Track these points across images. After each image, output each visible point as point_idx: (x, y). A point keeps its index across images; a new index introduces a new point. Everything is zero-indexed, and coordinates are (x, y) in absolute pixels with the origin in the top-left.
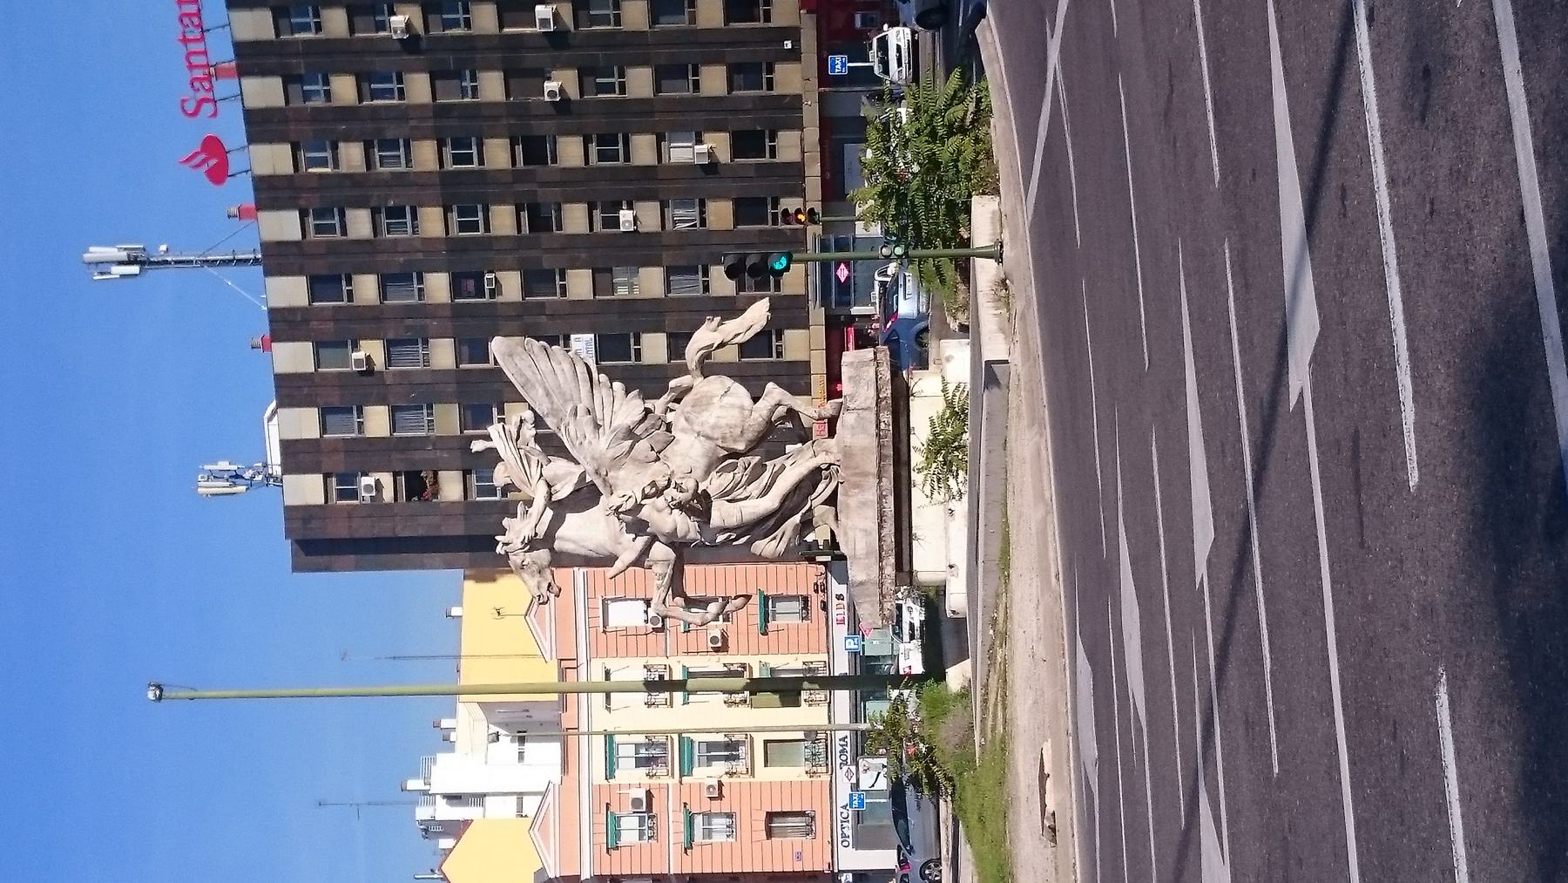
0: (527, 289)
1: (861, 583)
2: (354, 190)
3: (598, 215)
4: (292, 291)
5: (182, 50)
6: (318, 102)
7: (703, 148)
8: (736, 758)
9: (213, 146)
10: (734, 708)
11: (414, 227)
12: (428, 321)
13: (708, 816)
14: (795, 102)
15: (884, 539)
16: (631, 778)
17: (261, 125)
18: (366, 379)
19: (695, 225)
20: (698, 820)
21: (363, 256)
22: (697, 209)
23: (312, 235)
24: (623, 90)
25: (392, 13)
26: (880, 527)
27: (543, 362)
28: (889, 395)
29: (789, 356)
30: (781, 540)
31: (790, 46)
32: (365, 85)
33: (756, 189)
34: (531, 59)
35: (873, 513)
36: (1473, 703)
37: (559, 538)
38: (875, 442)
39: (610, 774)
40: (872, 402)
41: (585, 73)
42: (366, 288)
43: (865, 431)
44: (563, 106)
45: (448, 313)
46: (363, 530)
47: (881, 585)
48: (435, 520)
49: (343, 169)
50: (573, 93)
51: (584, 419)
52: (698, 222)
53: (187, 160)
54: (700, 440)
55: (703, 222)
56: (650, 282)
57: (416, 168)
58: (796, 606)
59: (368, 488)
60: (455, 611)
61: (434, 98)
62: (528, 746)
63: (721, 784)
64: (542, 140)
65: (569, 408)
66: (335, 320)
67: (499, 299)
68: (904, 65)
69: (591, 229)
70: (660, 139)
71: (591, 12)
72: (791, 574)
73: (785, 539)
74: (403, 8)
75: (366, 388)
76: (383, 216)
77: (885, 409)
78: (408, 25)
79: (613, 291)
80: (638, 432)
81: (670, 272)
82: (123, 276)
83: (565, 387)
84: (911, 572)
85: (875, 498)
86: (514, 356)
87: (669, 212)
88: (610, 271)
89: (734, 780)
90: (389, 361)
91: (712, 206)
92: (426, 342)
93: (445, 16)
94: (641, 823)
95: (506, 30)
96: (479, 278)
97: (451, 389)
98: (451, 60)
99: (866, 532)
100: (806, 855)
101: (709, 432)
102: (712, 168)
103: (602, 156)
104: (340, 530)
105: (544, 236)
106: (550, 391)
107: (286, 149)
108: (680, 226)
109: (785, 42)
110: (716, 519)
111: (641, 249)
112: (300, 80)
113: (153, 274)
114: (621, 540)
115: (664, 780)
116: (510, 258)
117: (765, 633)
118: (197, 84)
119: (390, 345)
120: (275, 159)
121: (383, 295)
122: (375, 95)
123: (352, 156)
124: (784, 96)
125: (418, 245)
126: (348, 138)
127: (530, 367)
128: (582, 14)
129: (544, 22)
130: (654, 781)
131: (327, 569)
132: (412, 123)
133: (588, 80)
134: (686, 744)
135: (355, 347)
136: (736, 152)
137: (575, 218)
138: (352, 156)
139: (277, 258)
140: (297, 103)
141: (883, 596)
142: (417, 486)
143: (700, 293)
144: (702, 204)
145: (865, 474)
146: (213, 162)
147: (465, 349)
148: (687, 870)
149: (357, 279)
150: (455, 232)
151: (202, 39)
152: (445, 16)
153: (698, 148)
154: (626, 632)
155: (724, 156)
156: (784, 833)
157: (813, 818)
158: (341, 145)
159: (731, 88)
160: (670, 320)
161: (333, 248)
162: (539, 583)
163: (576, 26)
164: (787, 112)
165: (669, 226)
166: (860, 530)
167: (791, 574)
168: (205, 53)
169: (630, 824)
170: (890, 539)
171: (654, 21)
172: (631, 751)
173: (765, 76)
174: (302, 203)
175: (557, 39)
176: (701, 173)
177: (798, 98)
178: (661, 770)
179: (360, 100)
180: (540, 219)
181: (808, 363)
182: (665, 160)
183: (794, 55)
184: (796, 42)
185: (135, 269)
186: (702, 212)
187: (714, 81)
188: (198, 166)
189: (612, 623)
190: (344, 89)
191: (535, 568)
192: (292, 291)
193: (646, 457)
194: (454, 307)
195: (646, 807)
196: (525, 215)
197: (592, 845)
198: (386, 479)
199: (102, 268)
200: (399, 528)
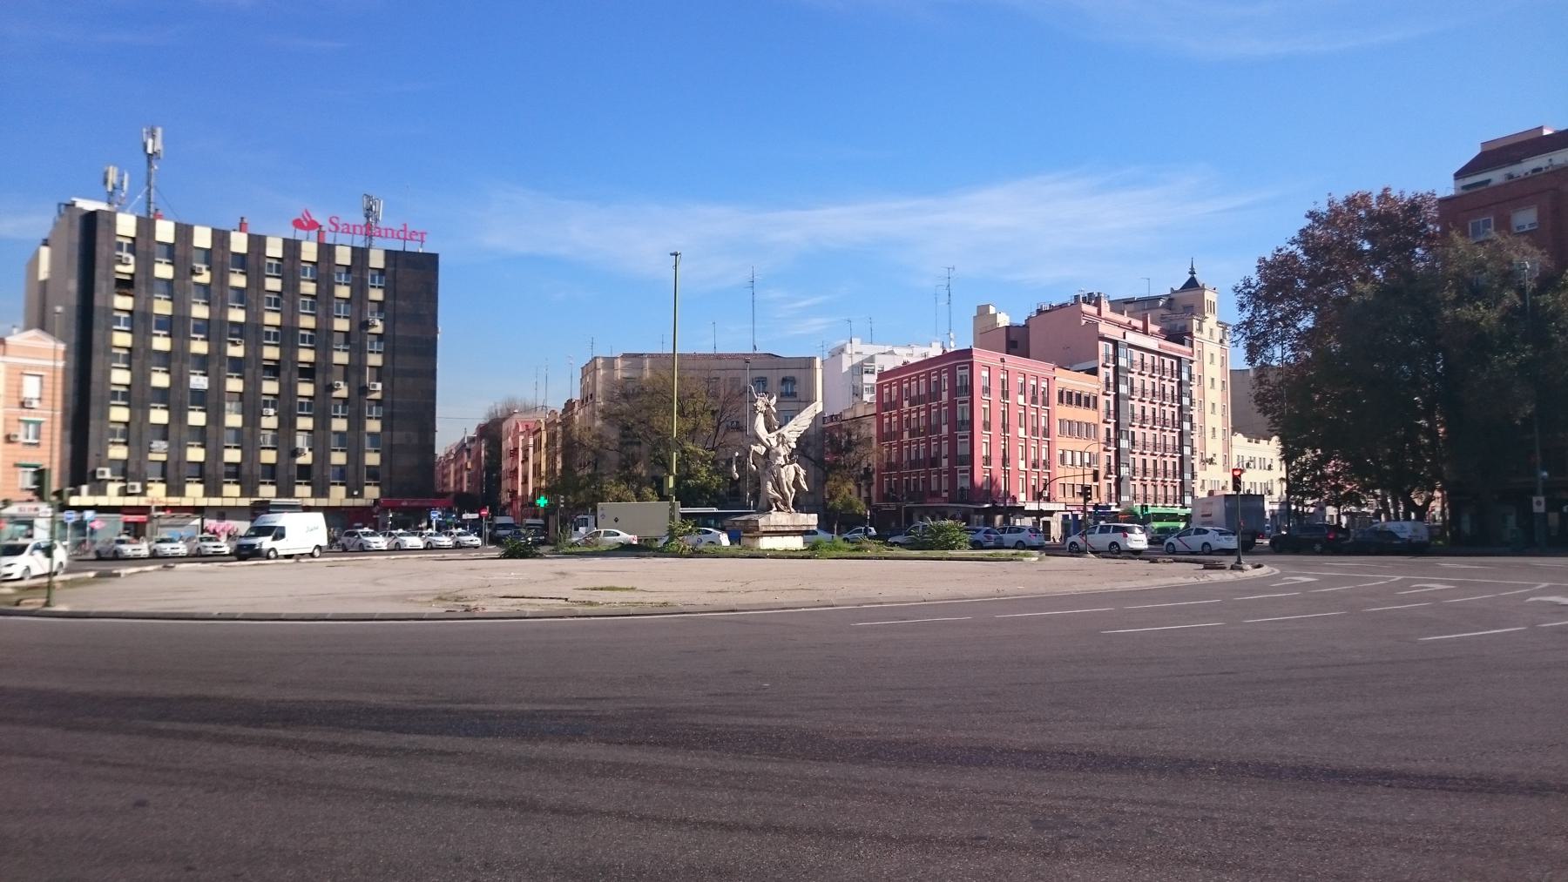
0: (233, 359)
2: (291, 285)
3: (271, 398)
11: (303, 314)
12: (219, 306)
18: (188, 271)
21: (256, 280)
23: (268, 261)
25: (381, 320)
33: (281, 474)
34: (354, 377)
35: (784, 523)
36: (813, 765)
41: (345, 401)
42: (238, 281)
48: (104, 291)
50: (335, 394)
55: (263, 448)
66: (222, 263)
70: (309, 431)
75: (185, 269)
78: (374, 326)
84: (762, 536)
87: (270, 433)
95: (368, 369)
97: (181, 313)
102: (295, 453)
105: (297, 374)
107: (314, 259)
113: (145, 158)
116: (251, 354)
118: (346, 226)
119: (206, 287)
121: (234, 288)
123: (309, 288)
125: (260, 310)
126: (318, 288)
129: (374, 386)
132: (325, 320)
133: (341, 402)
136: (301, 466)
137: (270, 387)
138: (309, 288)
142: (125, 286)
144: (273, 449)
146: (305, 223)
147: (199, 323)
154: (20, 387)
155: (300, 460)
164: (176, 489)
165: (263, 432)
174: (286, 260)
175: (364, 390)
182: (298, 433)
183: (349, 495)
184: (357, 497)
186: (268, 448)
194: (152, 313)
198: (130, 269)
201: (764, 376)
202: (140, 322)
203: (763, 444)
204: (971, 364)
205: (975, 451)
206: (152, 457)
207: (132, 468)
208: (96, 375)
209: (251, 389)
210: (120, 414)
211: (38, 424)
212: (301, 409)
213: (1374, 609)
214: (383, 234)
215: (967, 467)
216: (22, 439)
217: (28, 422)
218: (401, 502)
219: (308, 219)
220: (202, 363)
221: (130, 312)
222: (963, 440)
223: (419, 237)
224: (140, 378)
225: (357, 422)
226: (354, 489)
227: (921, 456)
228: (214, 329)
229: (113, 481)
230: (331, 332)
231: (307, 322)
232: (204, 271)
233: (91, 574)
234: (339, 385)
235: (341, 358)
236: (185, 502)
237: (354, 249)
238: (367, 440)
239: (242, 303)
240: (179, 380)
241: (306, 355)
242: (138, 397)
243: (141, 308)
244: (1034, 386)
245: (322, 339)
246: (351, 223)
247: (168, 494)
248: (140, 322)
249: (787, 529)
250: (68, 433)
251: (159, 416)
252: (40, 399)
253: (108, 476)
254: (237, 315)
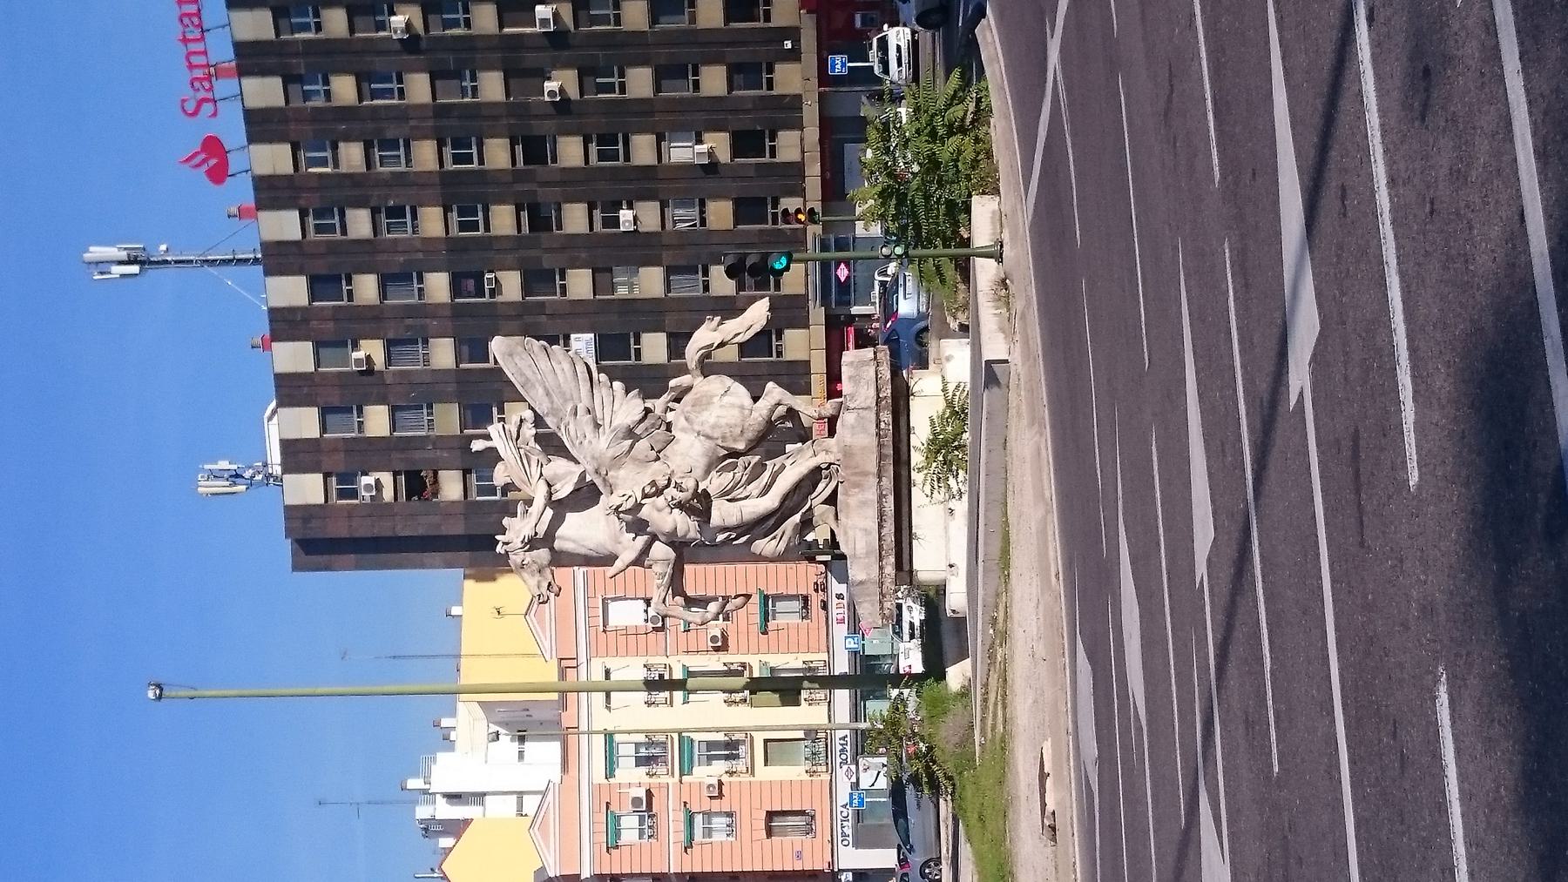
0: (527, 289)
1: (861, 583)
2: (354, 190)
3: (598, 215)
4: (292, 291)
5: (182, 50)
6: (318, 102)
7: (703, 148)
8: (736, 757)
9: (213, 146)
10: (734, 707)
11: (414, 227)
12: (428, 321)
13: (708, 815)
14: (795, 102)
15: (884, 538)
16: (631, 777)
17: (261, 125)
18: (366, 379)
19: (695, 225)
21: (363, 255)
22: (697, 208)
23: (312, 235)
24: (623, 90)
25: (392, 13)
26: (880, 527)
27: (543, 362)
28: (889, 395)
29: (789, 356)
30: (781, 539)
31: (790, 46)
32: (365, 85)
33: (756, 189)
34: (531, 59)
35: (873, 513)
37: (559, 537)
38: (875, 441)
39: (610, 773)
40: (872, 402)
41: (585, 73)
42: (366, 288)
43: (865, 430)
44: (563, 106)
45: (448, 313)
46: (363, 530)
47: (881, 584)
48: (435, 519)
49: (343, 169)
50: (573, 93)
51: (584, 418)
52: (698, 222)
53: (187, 160)
54: (700, 440)
55: (703, 222)
56: (650, 282)
57: (416, 168)
58: (796, 605)
59: (368, 487)
60: (455, 611)
61: (434, 98)
62: (528, 745)
63: (721, 784)
64: (542, 140)
65: (569, 407)
67: (499, 299)
68: (904, 65)
69: (591, 228)
70: (660, 138)
71: (591, 12)
72: (791, 573)
73: (785, 538)
74: (403, 8)
75: (366, 387)
76: (383, 215)
77: (885, 409)
78: (408, 25)
79: (613, 291)
80: (638, 431)
81: (670, 271)
82: (123, 276)
83: (565, 387)
84: (911, 571)
85: (875, 498)
86: (514, 356)
87: (669, 212)
88: (610, 270)
89: (734, 779)
90: (389, 360)
91: (712, 206)
92: (426, 342)
93: (445, 16)
94: (641, 822)
95: (506, 30)
96: (479, 278)
97: (451, 388)
98: (451, 60)
99: (866, 531)
100: (806, 854)
101: (709, 431)
102: (712, 168)
103: (602, 156)
104: (340, 530)
105: (544, 235)
106: (550, 391)
107: (286, 149)
108: (680, 226)
109: (785, 42)
110: (716, 519)
111: (641, 249)
112: (300, 80)
113: (153, 273)
114: (621, 539)
115: (664, 779)
116: (510, 258)
117: (765, 633)
118: (197, 84)
119: (390, 345)
121: (383, 294)
122: (375, 94)
123: (352, 156)
124: (784, 96)
125: (418, 245)
126: (348, 138)
127: (530, 366)
128: (582, 14)
129: (544, 22)
130: (654, 780)
131: (327, 568)
132: (412, 123)
133: (588, 80)
134: (686, 744)
135: (355, 347)
136: (736, 151)
137: (575, 218)
138: (352, 156)
139: (277, 258)
140: (297, 103)
141: (883, 595)
142: (417, 485)
143: (700, 293)
144: (702, 204)
145: (865, 474)
146: (213, 162)
147: (465, 349)
148: (687, 869)
149: (357, 278)
150: (455, 231)
151: (202, 39)
152: (445, 16)
153: (698, 148)
154: (626, 632)
155: (724, 156)
156: (784, 832)
158: (341, 145)
159: (731, 88)
160: (670, 320)
161: (333, 248)
162: (539, 582)
163: (576, 26)
164: (787, 111)
165: (669, 225)
166: (860, 529)
167: (791, 573)
168: (205, 53)
169: (630, 823)
170: (890, 539)
171: (654, 21)
172: (631, 750)
173: (765, 76)
174: (302, 202)
175: (557, 39)
176: (701, 173)
177: (798, 98)
178: (661, 770)
179: (360, 100)
180: (540, 219)
181: (808, 363)
182: (665, 160)
183: (794, 55)
184: (796, 42)
185: (135, 269)
186: (702, 212)
187: (714, 81)
188: (198, 166)
189: (612, 623)
190: (344, 89)
191: (535, 567)
192: (292, 291)
193: (646, 456)
194: (454, 307)
195: (646, 806)
196: (525, 215)
197: (592, 844)
198: (386, 478)
199: (102, 267)
200: (399, 527)
219: (202, 156)
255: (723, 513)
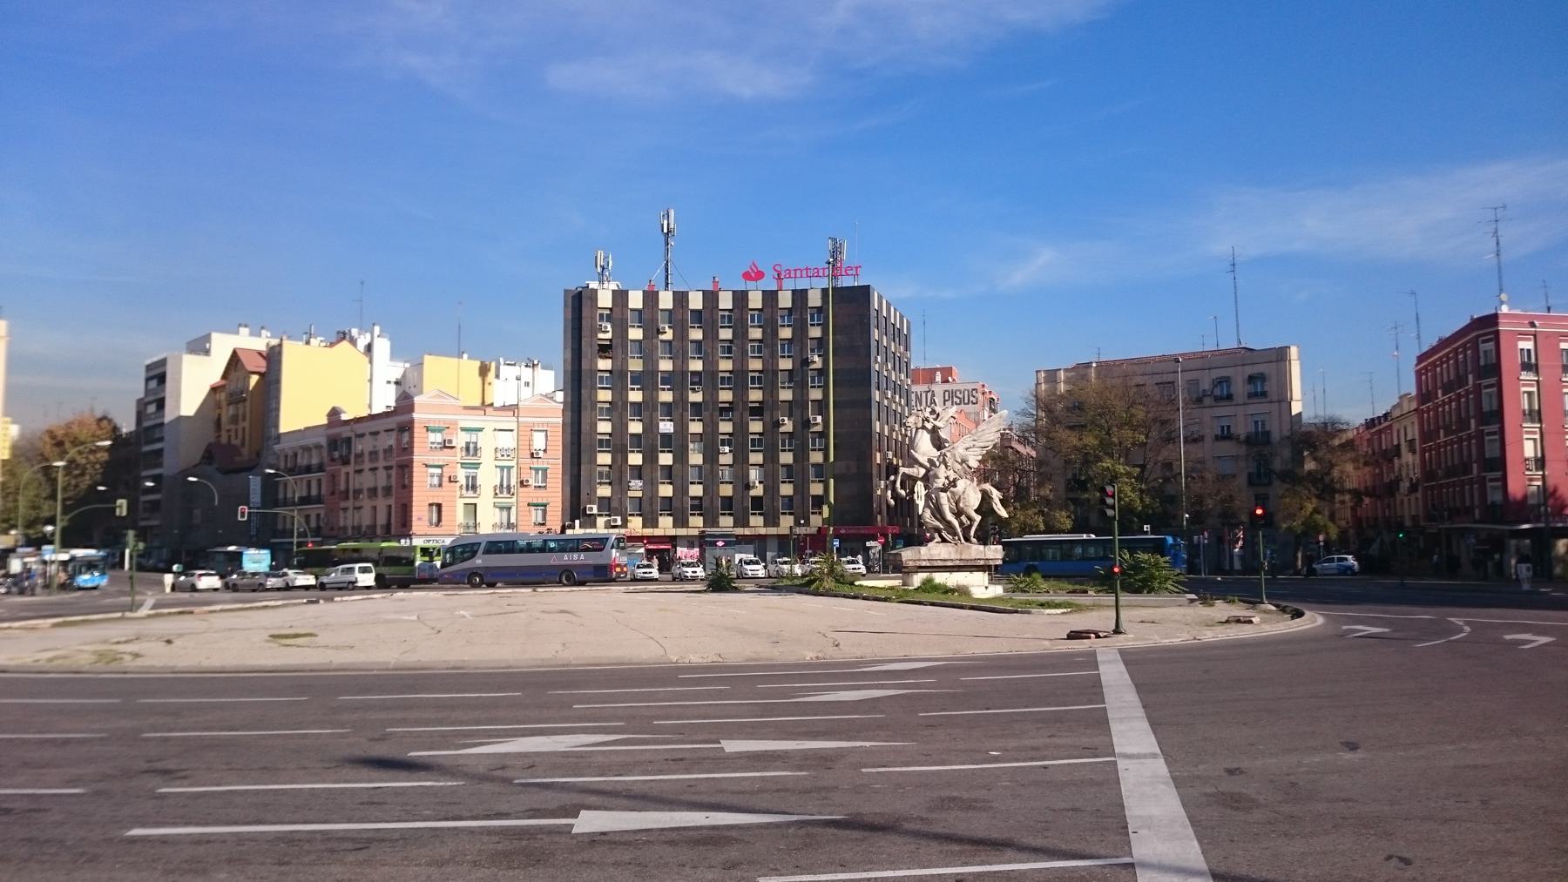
0: (694, 404)
4: (696, 302)
5: (803, 267)
6: (780, 323)
7: (757, 484)
8: (467, 489)
9: (760, 275)
10: (493, 489)
11: (723, 358)
13: (441, 477)
14: (776, 524)
16: (460, 440)
17: (770, 297)
20: (439, 471)
21: (711, 334)
23: (721, 313)
25: (819, 356)
27: (995, 429)
29: (661, 519)
32: (787, 342)
34: (797, 412)
35: (946, 557)
38: (973, 558)
39: (463, 429)
42: (696, 334)
43: (978, 554)
44: (777, 424)
46: (586, 323)
47: (919, 560)
49: (750, 330)
50: (782, 429)
53: (753, 264)
55: (722, 483)
56: (696, 458)
58: (540, 520)
59: (606, 327)
60: (465, 356)
61: (781, 371)
62: (393, 386)
63: (456, 482)
67: (690, 392)
70: (760, 466)
72: (556, 518)
74: (821, 360)
75: (652, 331)
78: (814, 362)
80: (964, 465)
81: (700, 467)
82: (663, 225)
84: (917, 572)
87: (727, 468)
89: (458, 489)
90: (662, 341)
91: (730, 486)
92: (671, 358)
94: (439, 443)
99: (939, 555)
100: (420, 523)
102: (748, 487)
104: (586, 312)
108: (720, 472)
111: (711, 456)
112: (790, 315)
113: (663, 238)
115: (459, 455)
116: (708, 398)
117: (529, 505)
118: (816, 271)
119: (670, 342)
120: (756, 301)
122: (783, 346)
123: (756, 333)
126: (764, 333)
129: (815, 419)
130: (459, 450)
131: (565, 305)
133: (787, 436)
134: (477, 466)
135: (670, 327)
137: (726, 427)
139: (711, 297)
140: (779, 312)
141: (915, 561)
142: (605, 350)
144: (731, 483)
145: (961, 554)
146: (753, 275)
147: (667, 375)
148: (415, 464)
149: (701, 331)
151: (807, 276)
153: (757, 482)
155: (753, 493)
156: (431, 512)
157: (437, 525)
158: (761, 330)
159: (783, 497)
160: (678, 466)
161: (714, 322)
164: (772, 521)
165: (721, 468)
167: (556, 518)
168: (801, 277)
169: (438, 438)
170: (936, 564)
171: (813, 465)
172: (474, 440)
173: (788, 511)
174: (765, 310)
175: (807, 424)
176: (745, 482)
177: (778, 525)
178: (464, 453)
179: (781, 339)
180: (726, 411)
181: (657, 527)
182: (750, 467)
185: (665, 231)
186: (727, 483)
187: (786, 490)
188: (752, 269)
189: (535, 434)
190: (786, 333)
192: (696, 302)
195: (446, 445)
196: (727, 405)
197: (429, 421)
198: (609, 336)
199: (666, 216)
200: (586, 339)
201: (1261, 370)
202: (618, 379)
203: (922, 465)
204: (1497, 333)
205: (1508, 448)
206: (631, 494)
207: (614, 504)
208: (585, 427)
209: (709, 430)
210: (604, 459)
211: (545, 471)
212: (601, 446)
213: (867, 744)
214: (821, 274)
215: (1498, 474)
216: (532, 482)
217: (537, 470)
218: (841, 529)
220: (668, 409)
221: (610, 372)
222: (1492, 437)
223: (854, 272)
224: (619, 428)
225: (801, 455)
226: (802, 517)
227: (1456, 462)
228: (678, 380)
229: (601, 515)
230: (684, 373)
231: (755, 365)
232: (667, 329)
233: (305, 601)
234: (783, 420)
235: (786, 395)
236: (658, 532)
237: (704, 292)
238: (811, 471)
239: (641, 354)
240: (650, 427)
241: (755, 395)
242: (618, 444)
243: (739, 367)
244: (1529, 351)
245: (768, 378)
246: (792, 269)
247: (644, 526)
248: (618, 379)
249: (949, 564)
250: (568, 477)
251: (635, 459)
252: (545, 451)
253: (595, 511)
254: (696, 365)
255: (944, 497)
